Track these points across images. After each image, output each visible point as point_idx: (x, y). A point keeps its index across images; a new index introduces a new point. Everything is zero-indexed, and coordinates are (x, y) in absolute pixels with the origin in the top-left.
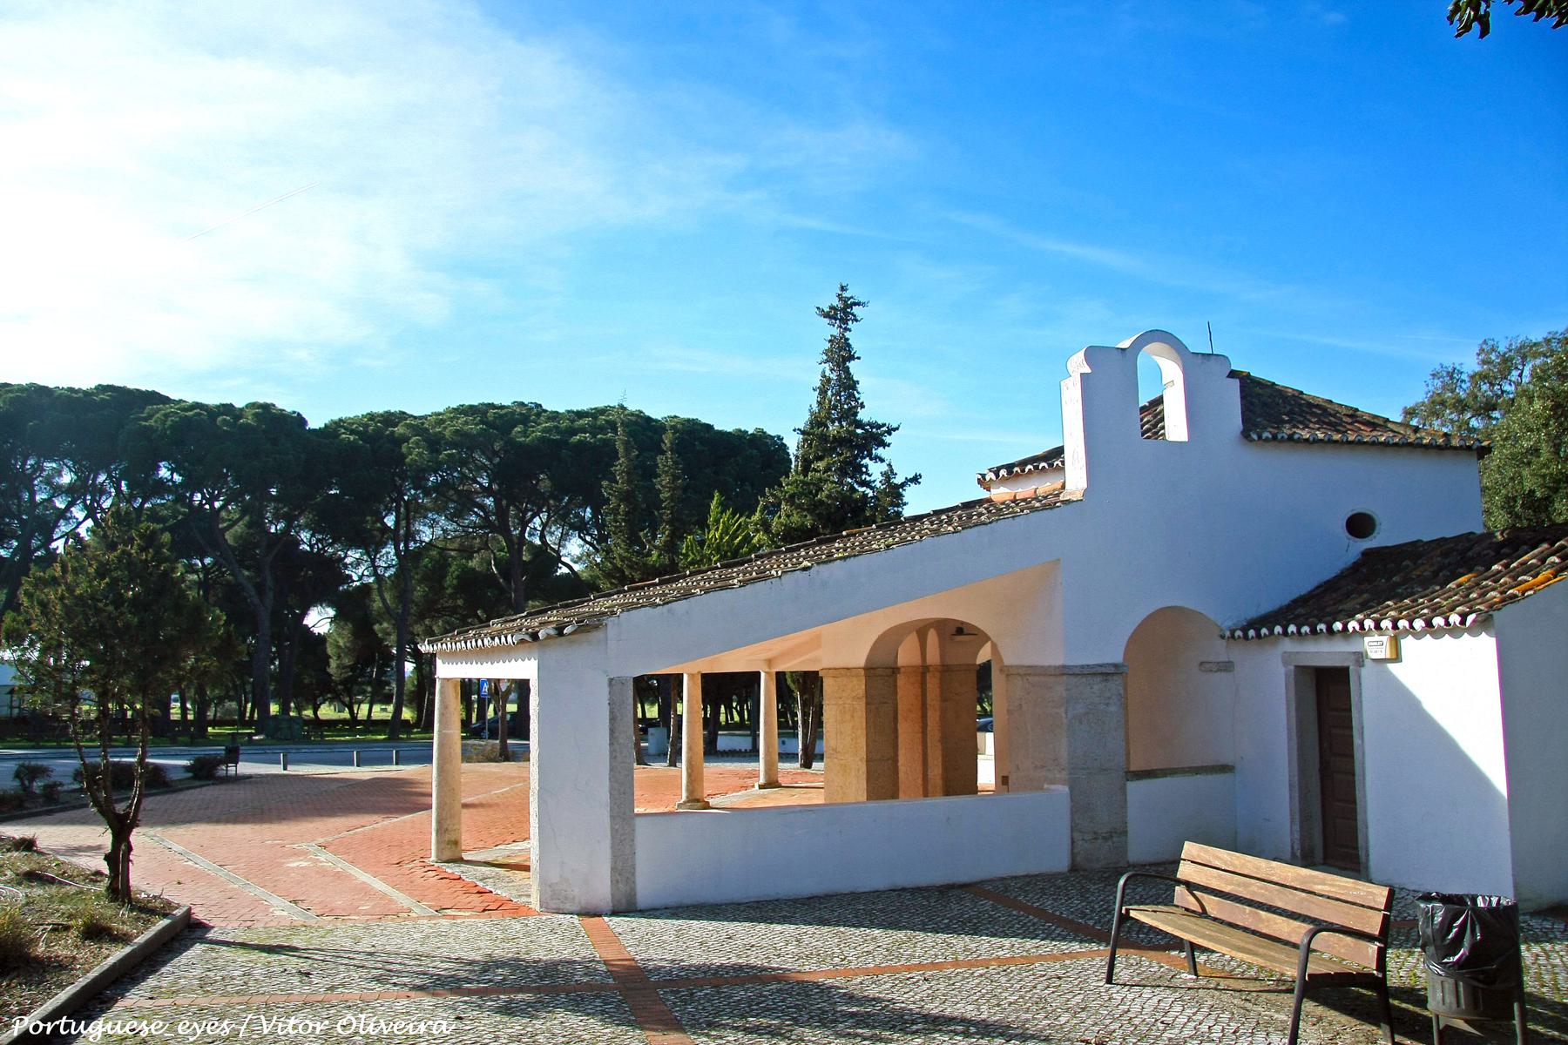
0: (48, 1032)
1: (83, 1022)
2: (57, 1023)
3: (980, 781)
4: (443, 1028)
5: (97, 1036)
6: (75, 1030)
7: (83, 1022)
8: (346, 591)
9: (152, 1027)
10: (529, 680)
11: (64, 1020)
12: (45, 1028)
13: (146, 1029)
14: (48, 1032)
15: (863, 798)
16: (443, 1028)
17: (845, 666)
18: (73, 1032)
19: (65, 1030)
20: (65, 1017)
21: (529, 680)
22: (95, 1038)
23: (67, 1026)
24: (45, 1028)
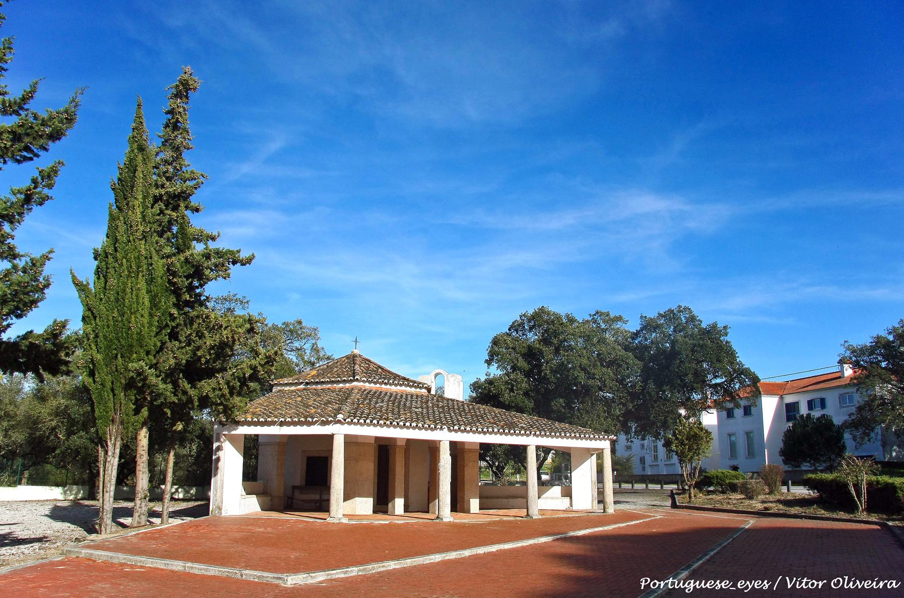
0: (820, 587)
1: (704, 581)
2: (667, 581)
3: (478, 500)
4: (894, 584)
5: (690, 589)
6: (677, 586)
7: (704, 581)
8: (175, 430)
9: (723, 584)
10: (808, 401)
11: (671, 580)
12: (818, 585)
13: (719, 586)
14: (820, 587)
15: (370, 512)
16: (894, 584)
17: (25, 500)
18: (676, 587)
19: (671, 586)
20: (671, 578)
21: (808, 401)
22: (689, 590)
23: (673, 583)
24: (818, 585)
